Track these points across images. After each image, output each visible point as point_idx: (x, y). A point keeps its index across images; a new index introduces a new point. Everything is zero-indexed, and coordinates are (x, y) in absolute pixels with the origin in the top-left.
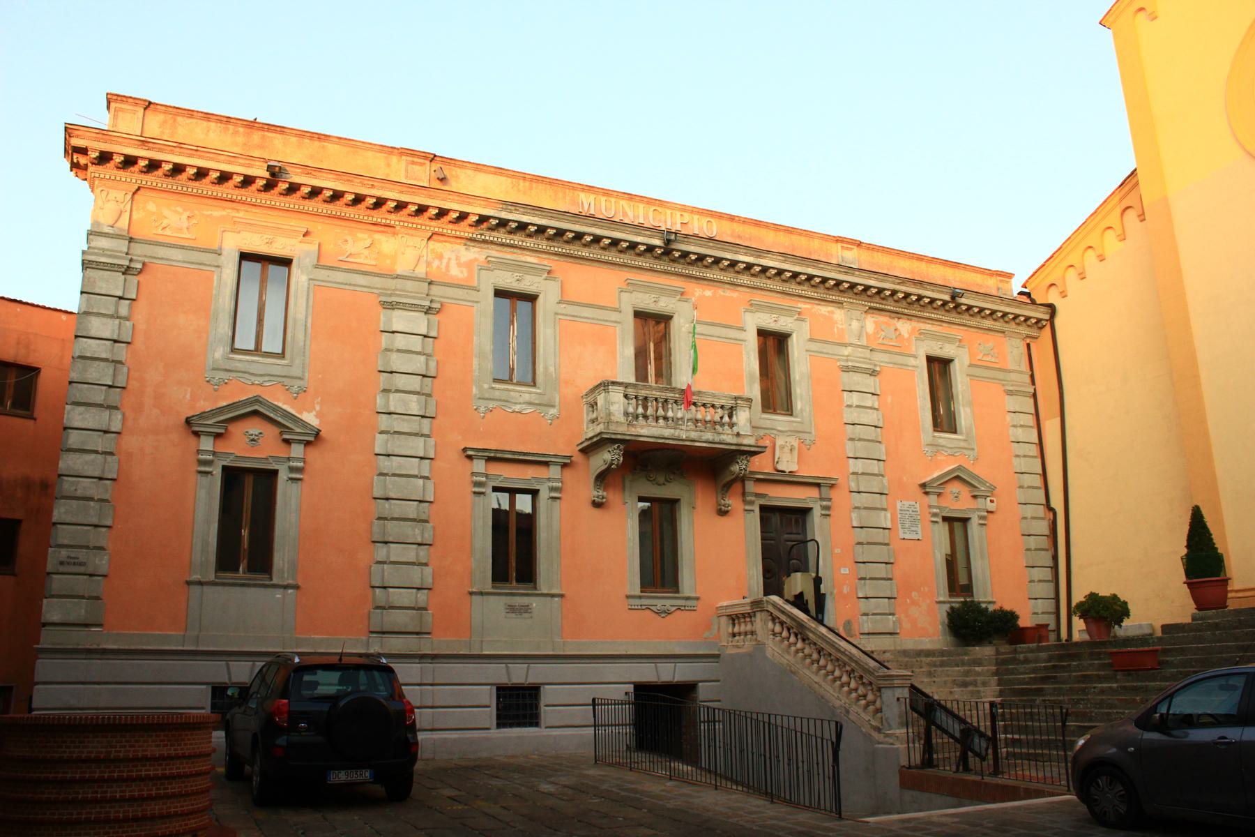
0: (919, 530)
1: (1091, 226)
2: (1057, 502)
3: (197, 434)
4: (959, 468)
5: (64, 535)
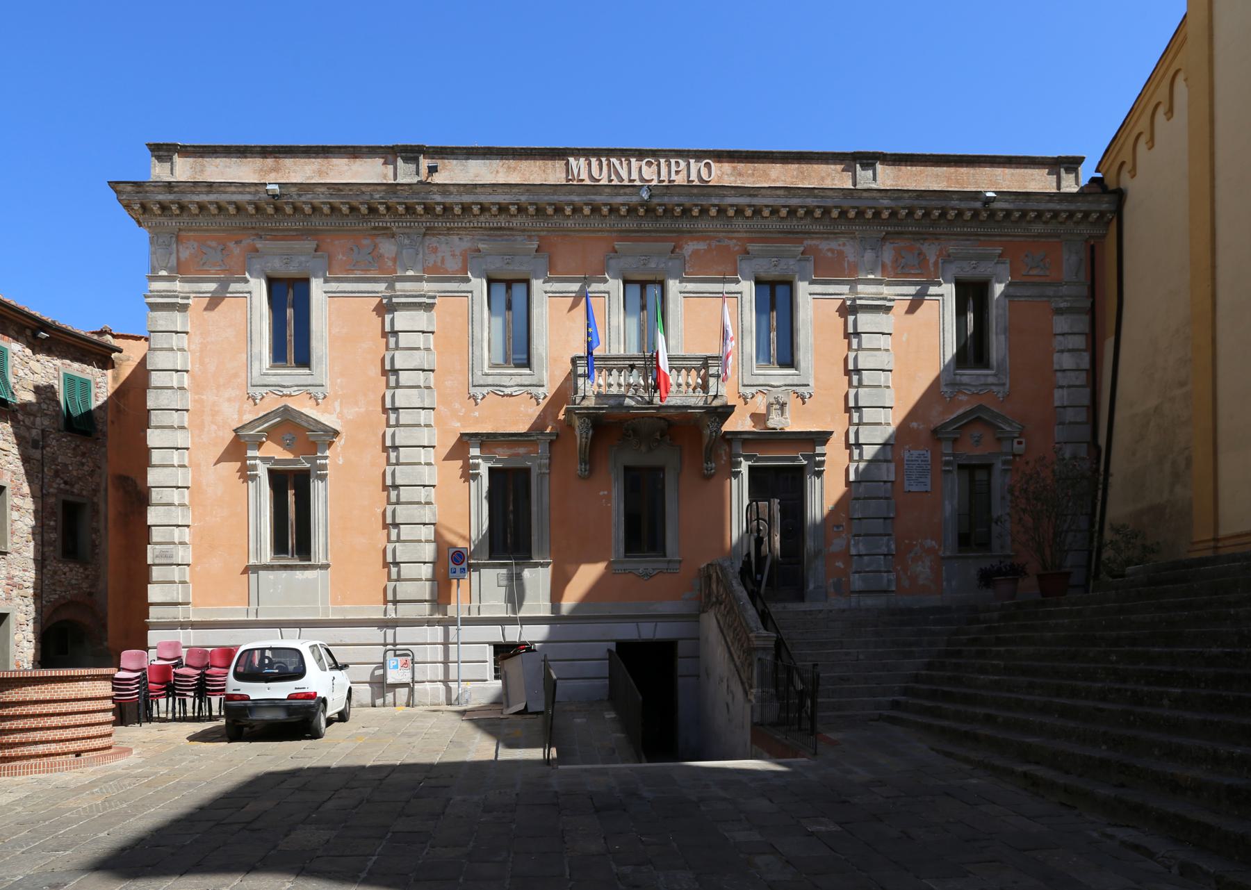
0: (928, 481)
1: (1176, 47)
2: (1102, 441)
3: (939, 440)
4: (980, 408)
5: (156, 534)
